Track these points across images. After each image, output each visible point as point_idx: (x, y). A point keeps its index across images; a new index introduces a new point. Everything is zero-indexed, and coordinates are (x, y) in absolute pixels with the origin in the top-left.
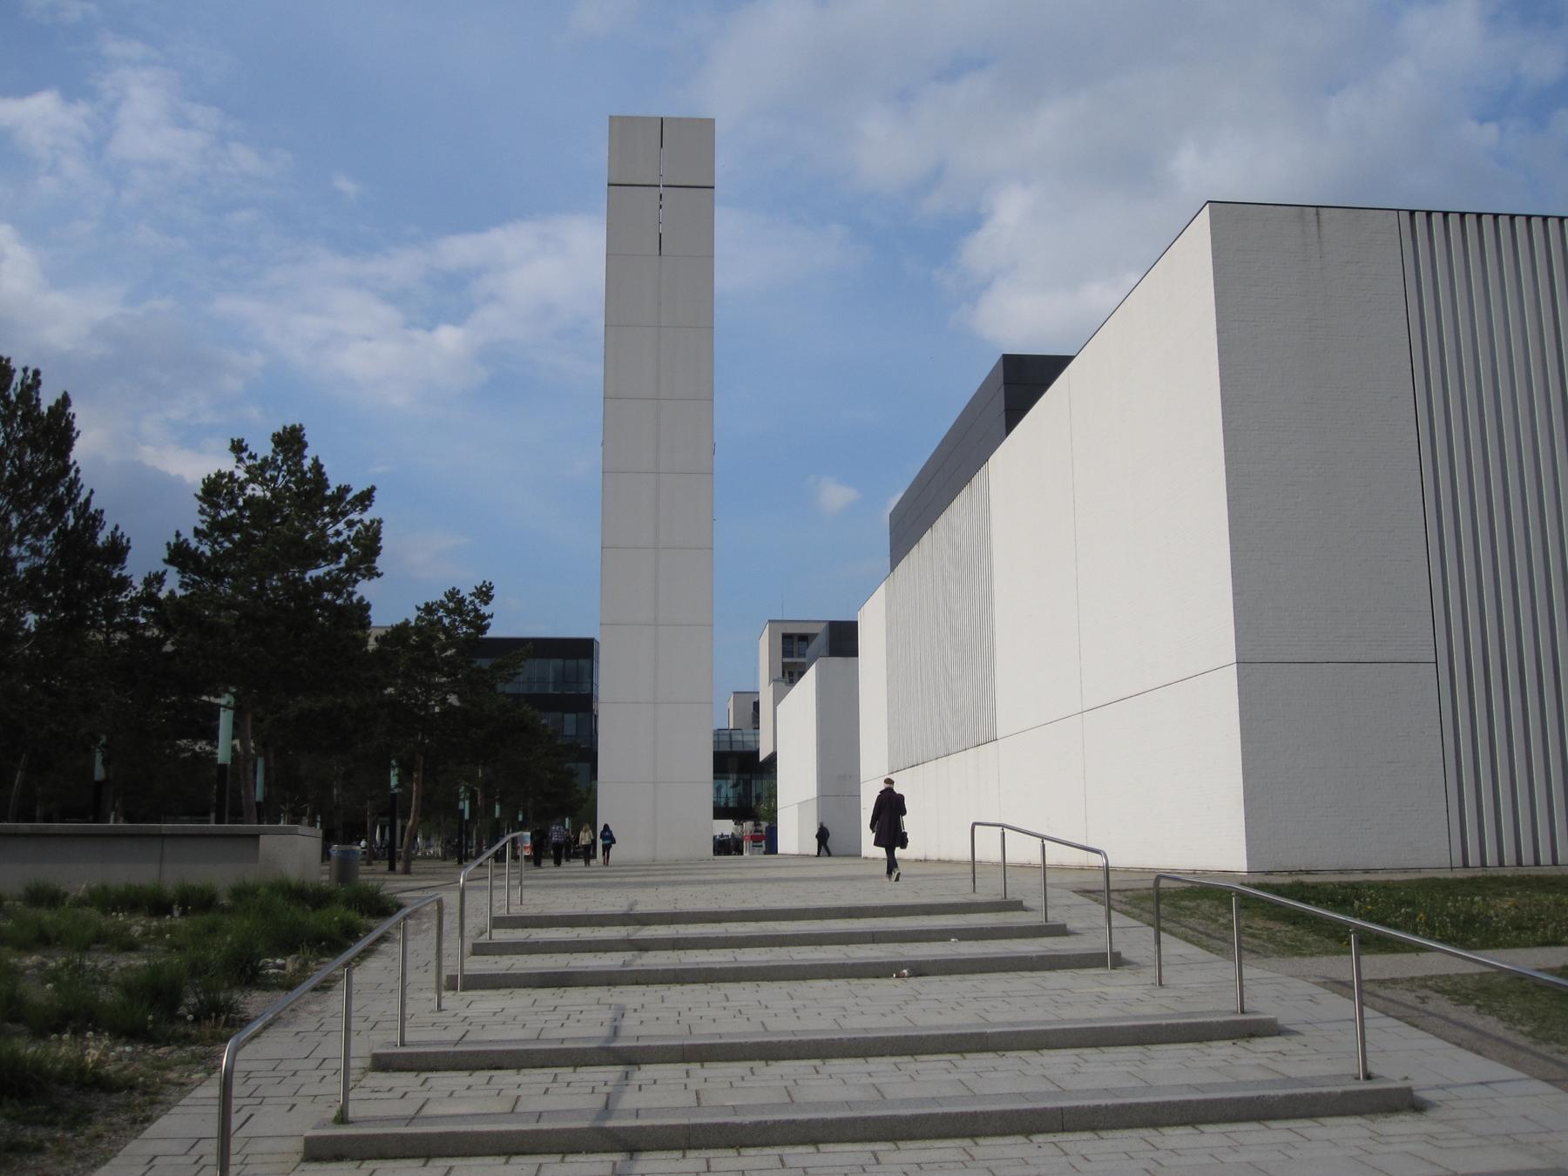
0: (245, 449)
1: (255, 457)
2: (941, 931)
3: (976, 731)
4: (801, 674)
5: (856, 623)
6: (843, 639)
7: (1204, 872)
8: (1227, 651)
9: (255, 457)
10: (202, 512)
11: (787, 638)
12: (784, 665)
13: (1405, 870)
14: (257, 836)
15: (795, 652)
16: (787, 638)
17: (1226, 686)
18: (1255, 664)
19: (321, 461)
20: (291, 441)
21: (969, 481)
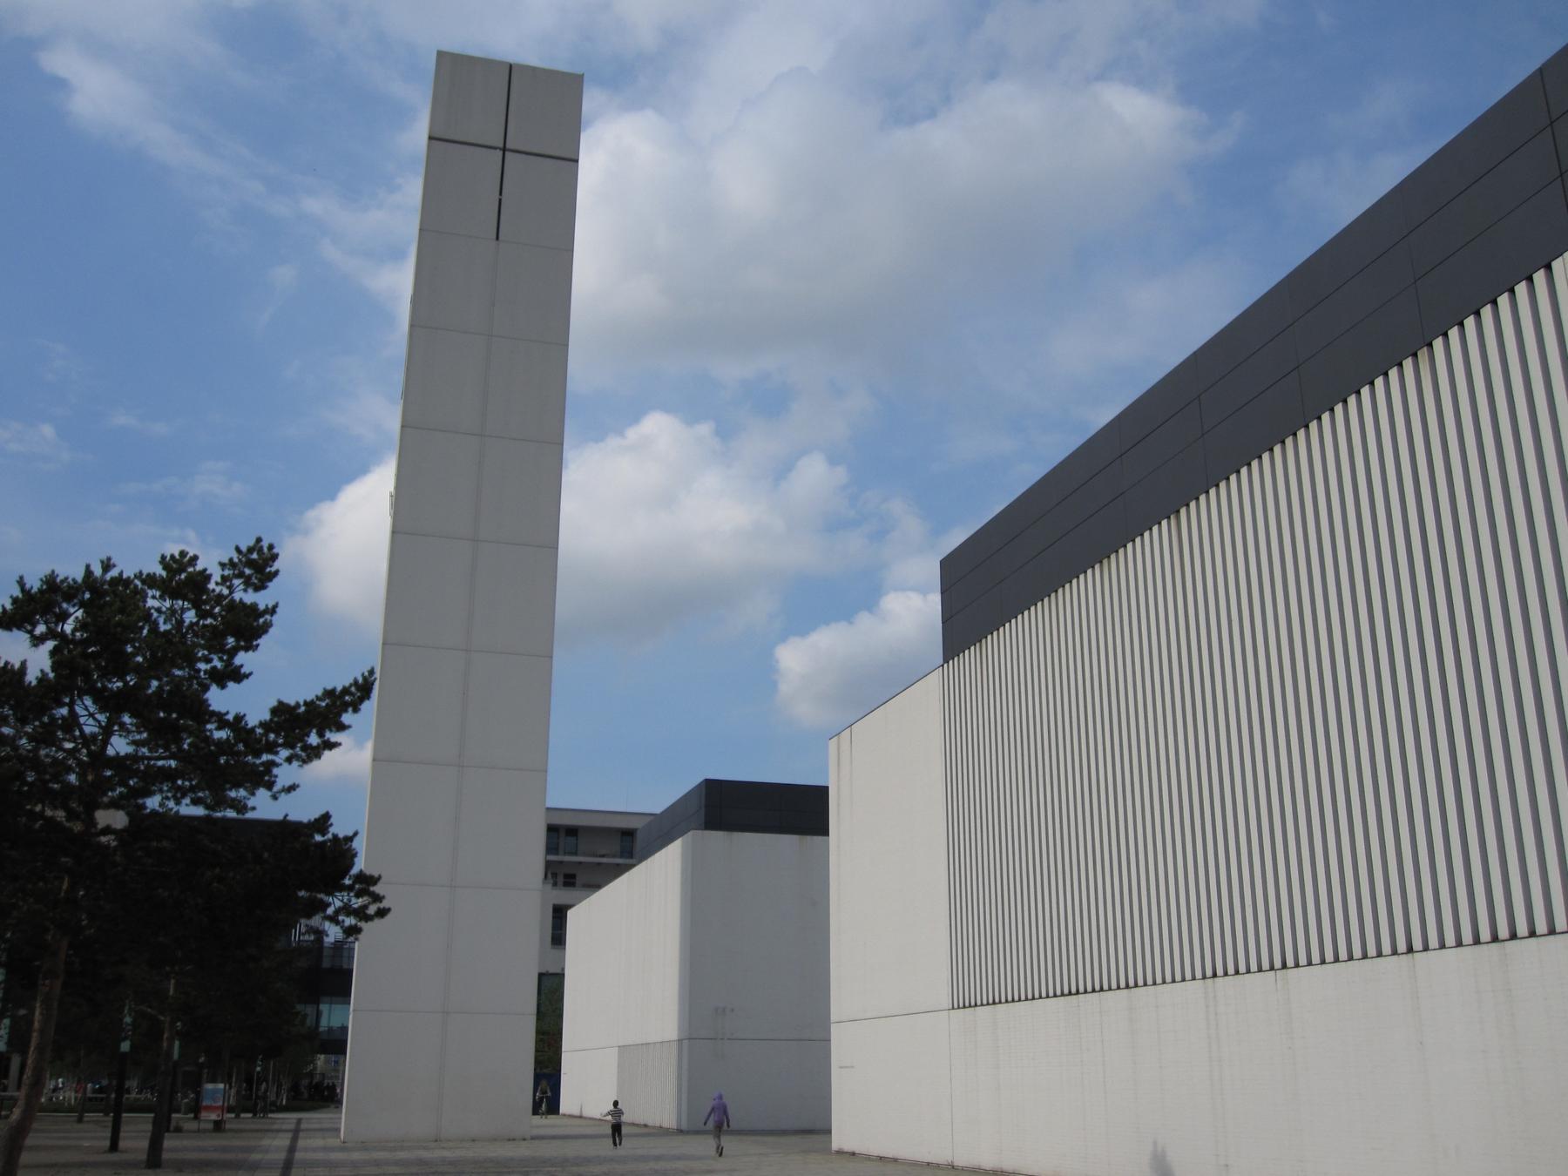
12: (548, 864)
15: (586, 853)
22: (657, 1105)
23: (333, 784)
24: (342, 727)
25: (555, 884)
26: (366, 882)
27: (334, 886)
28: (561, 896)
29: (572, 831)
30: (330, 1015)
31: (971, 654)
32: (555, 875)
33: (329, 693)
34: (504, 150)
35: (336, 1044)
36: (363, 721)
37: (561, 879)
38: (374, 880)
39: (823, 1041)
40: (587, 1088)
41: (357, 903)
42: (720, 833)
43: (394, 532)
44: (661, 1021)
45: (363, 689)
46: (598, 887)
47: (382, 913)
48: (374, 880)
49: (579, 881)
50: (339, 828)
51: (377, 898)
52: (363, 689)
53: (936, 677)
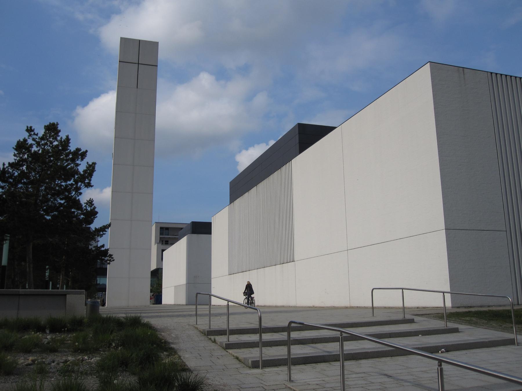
0: (33, 131)
1: (37, 135)
2: (415, 332)
3: (287, 257)
4: (176, 240)
5: (211, 223)
6: (203, 228)
7: (424, 308)
8: (442, 225)
9: (37, 135)
10: (15, 155)
11: (161, 228)
12: (160, 238)
13: (500, 306)
14: (65, 295)
15: (168, 235)
16: (161, 228)
17: (442, 236)
18: (450, 230)
19: (70, 137)
20: (52, 129)
21: (280, 168)
22: (182, 300)
23: (105, 241)
24: (106, 231)
25: (162, 244)
26: (111, 256)
27: (106, 256)
28: (163, 247)
29: (167, 229)
30: (100, 281)
31: (232, 204)
32: (162, 241)
33: (104, 226)
34: (138, 64)
35: (103, 289)
36: (109, 230)
37: (164, 242)
38: (112, 255)
39: (210, 283)
40: (169, 296)
41: (109, 259)
42: (195, 235)
43: (116, 112)
44: (182, 280)
45: (110, 225)
46: (172, 244)
47: (113, 260)
48: (112, 255)
49: (169, 242)
50: (106, 247)
51: (113, 258)
52: (110, 225)
53: (226, 209)
